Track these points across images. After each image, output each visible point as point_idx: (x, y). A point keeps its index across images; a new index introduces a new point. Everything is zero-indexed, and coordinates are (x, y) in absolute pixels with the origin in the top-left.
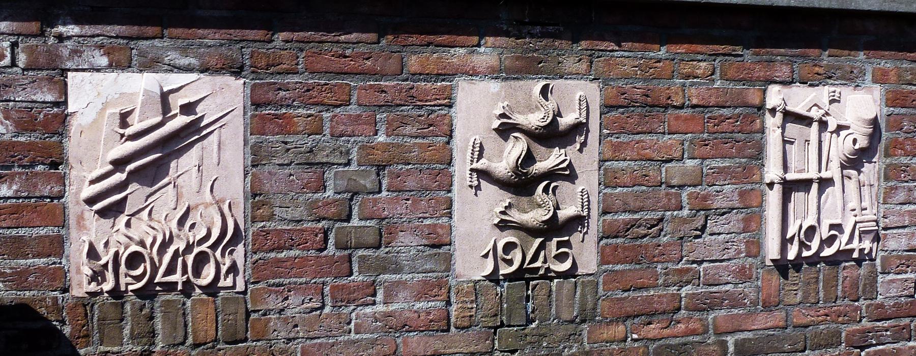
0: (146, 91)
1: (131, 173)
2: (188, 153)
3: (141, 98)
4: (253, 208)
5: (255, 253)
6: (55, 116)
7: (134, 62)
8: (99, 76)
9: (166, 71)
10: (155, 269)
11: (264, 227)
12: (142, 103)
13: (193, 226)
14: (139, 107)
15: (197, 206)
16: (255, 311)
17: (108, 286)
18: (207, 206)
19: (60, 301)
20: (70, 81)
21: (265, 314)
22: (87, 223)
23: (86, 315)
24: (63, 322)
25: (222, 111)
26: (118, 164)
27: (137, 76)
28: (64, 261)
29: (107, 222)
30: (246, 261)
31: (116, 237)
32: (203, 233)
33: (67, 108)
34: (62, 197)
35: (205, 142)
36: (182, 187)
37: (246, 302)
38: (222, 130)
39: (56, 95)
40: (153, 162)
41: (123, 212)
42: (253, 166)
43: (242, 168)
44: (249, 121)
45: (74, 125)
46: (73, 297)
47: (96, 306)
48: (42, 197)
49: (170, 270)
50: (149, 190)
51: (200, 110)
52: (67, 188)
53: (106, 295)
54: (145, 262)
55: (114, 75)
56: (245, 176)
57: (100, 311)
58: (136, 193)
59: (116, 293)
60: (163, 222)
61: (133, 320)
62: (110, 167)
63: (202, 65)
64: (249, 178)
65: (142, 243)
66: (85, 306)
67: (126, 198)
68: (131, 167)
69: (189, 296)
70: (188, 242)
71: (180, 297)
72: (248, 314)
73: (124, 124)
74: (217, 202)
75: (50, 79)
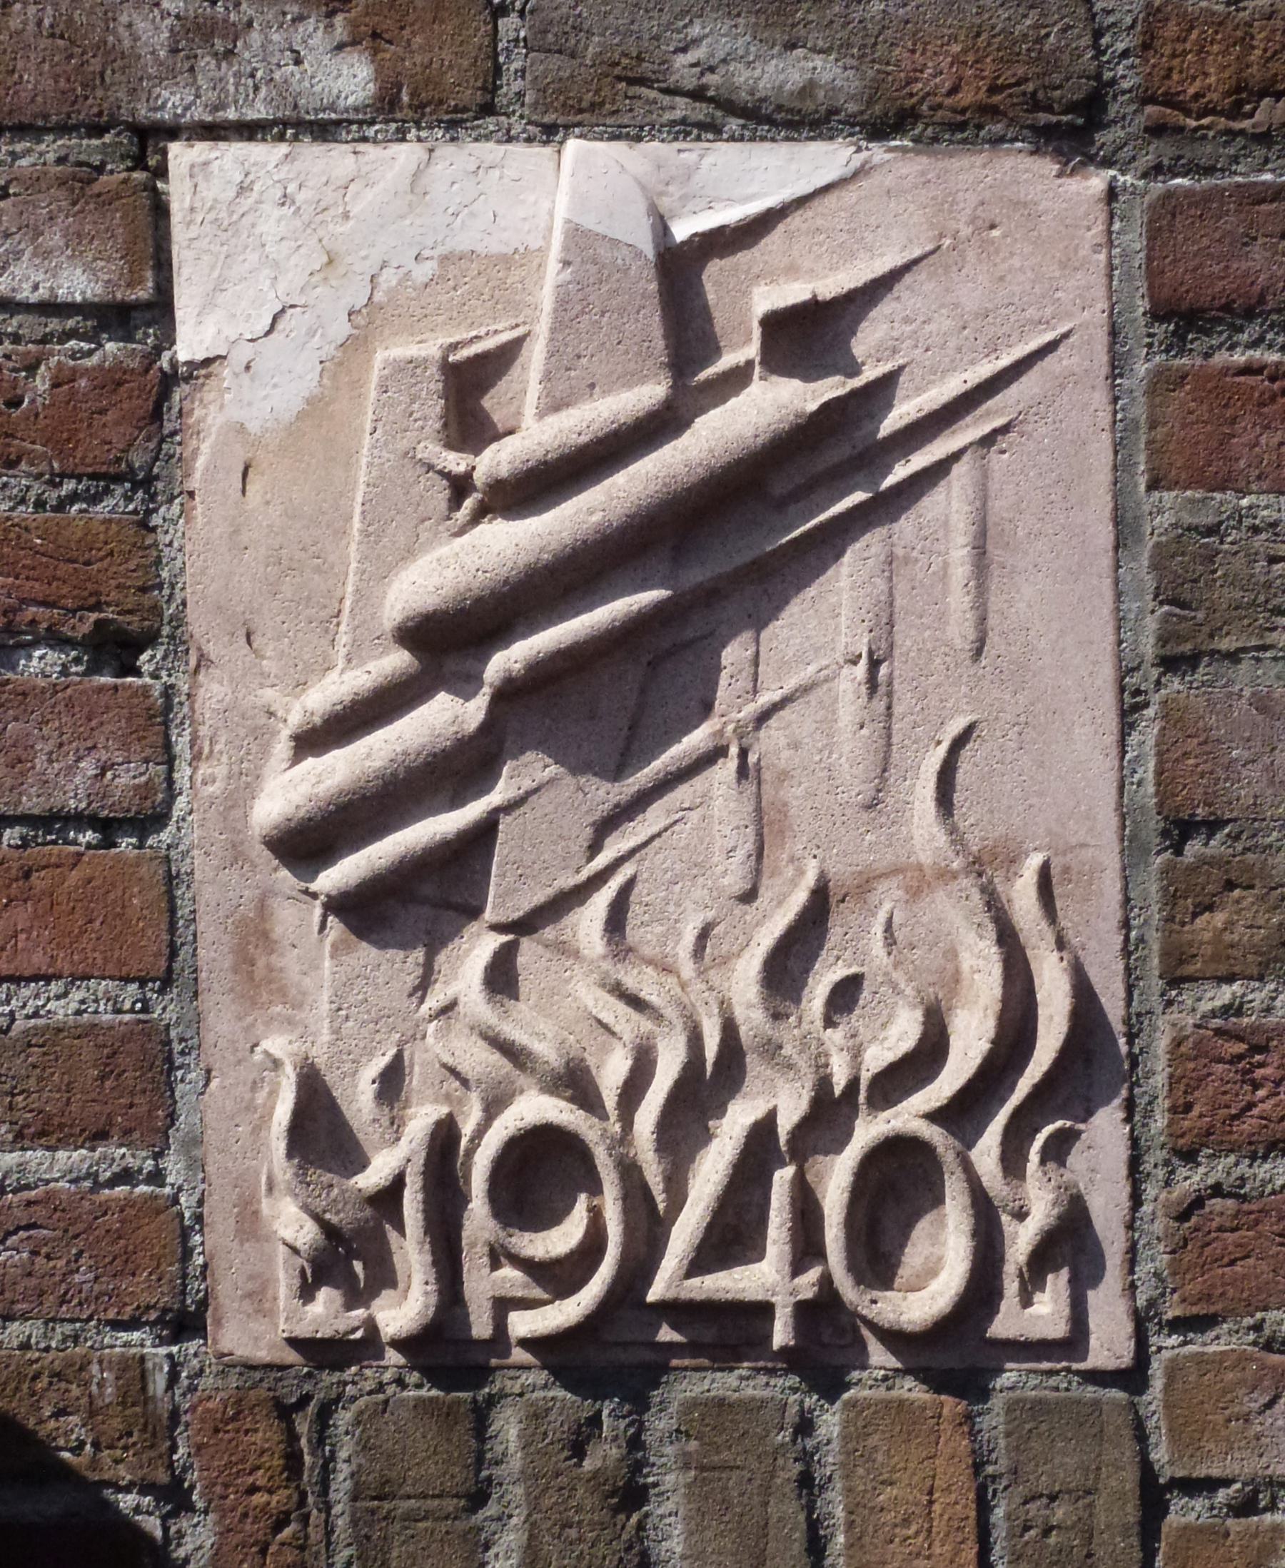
0: (578, 238)
1: (510, 694)
2: (811, 591)
3: (553, 273)
4: (1171, 899)
5: (1189, 1156)
6: (112, 379)
7: (510, 86)
8: (335, 160)
9: (684, 130)
10: (648, 1229)
11: (1234, 1009)
12: (562, 303)
13: (845, 996)
14: (542, 328)
15: (865, 884)
16: (1191, 1486)
17: (401, 1312)
18: (920, 882)
19: (158, 1383)
20: (178, 192)
21: (1246, 1507)
22: (290, 963)
23: (293, 1461)
24: (175, 1498)
25: (993, 350)
26: (446, 641)
27: (527, 159)
28: (174, 1167)
29: (400, 965)
30: (1136, 1199)
31: (436, 1046)
32: (901, 1034)
33: (168, 338)
34: (159, 819)
35: (906, 526)
36: (784, 776)
37: (1141, 1435)
38: (998, 461)
39: (112, 269)
40: (631, 627)
41: (474, 912)
42: (1170, 664)
43: (1106, 673)
44: (1140, 411)
45: (216, 425)
46: (227, 1363)
47: (343, 1418)
48: (54, 821)
49: (730, 1237)
50: (605, 794)
51: (872, 344)
52: (183, 774)
53: (393, 1357)
54: (595, 1188)
55: (406, 154)
56: (1128, 715)
57: (364, 1446)
58: (540, 807)
59: (447, 1351)
60: (687, 969)
61: (534, 1504)
62: (398, 661)
63: (873, 93)
64: (1147, 734)
65: (575, 1083)
66: (285, 1412)
67: (484, 832)
68: (507, 660)
69: (829, 1383)
70: (823, 1083)
71: (782, 1389)
72: (1153, 1496)
73: (468, 422)
74: (977, 866)
75: (81, 179)
